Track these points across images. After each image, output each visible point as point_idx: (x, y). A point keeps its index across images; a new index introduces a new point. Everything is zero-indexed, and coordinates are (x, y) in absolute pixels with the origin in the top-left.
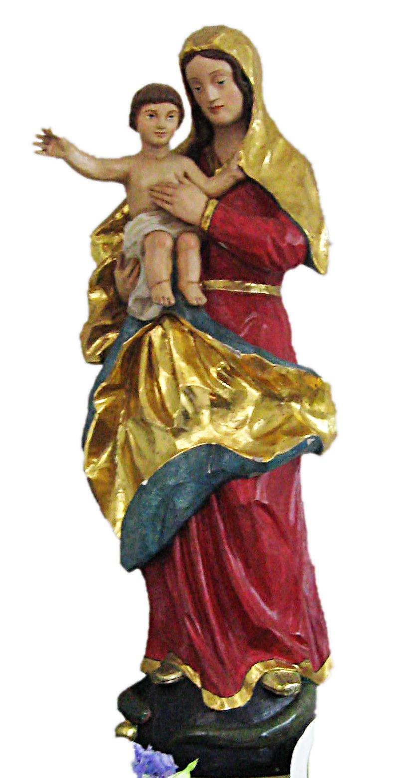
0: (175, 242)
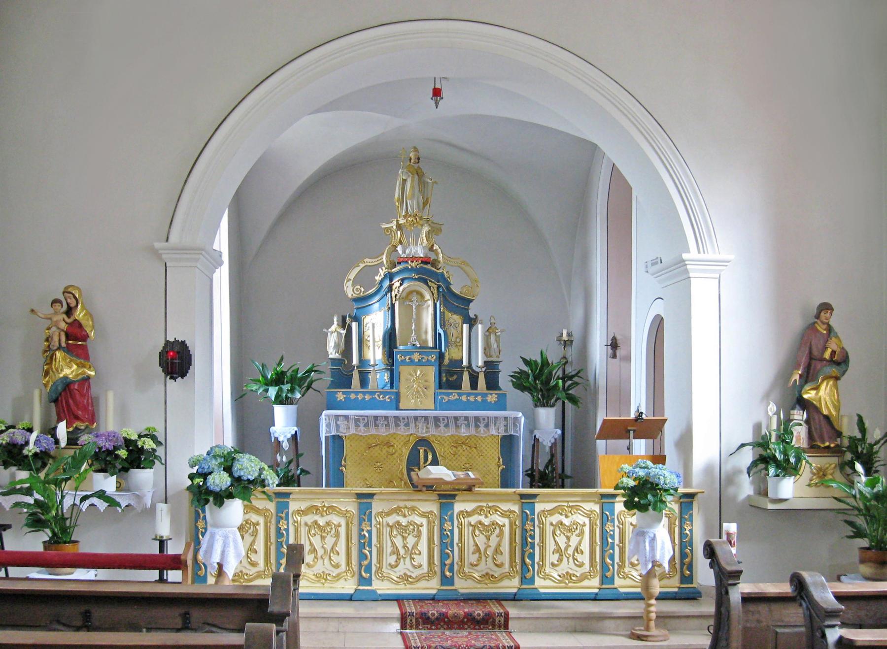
0: (59, 333)
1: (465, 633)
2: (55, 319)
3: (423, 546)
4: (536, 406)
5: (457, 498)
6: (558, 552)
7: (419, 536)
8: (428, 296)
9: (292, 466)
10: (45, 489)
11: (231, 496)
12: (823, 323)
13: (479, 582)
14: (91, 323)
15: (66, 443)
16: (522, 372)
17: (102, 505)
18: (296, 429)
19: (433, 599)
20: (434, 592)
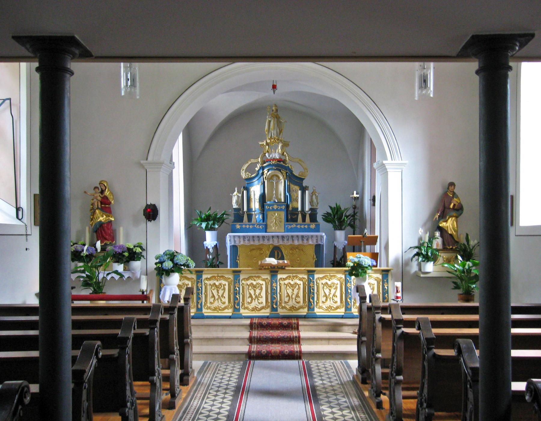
1: (279, 332)
2: (96, 195)
3: (263, 294)
4: (335, 230)
5: (279, 272)
6: (325, 296)
7: (261, 289)
8: (281, 177)
9: (214, 261)
10: (91, 270)
11: (173, 271)
12: (451, 192)
13: (289, 310)
14: (112, 197)
15: (100, 250)
16: (328, 213)
17: (117, 277)
18: (216, 242)
19: (268, 317)
20: (268, 314)
